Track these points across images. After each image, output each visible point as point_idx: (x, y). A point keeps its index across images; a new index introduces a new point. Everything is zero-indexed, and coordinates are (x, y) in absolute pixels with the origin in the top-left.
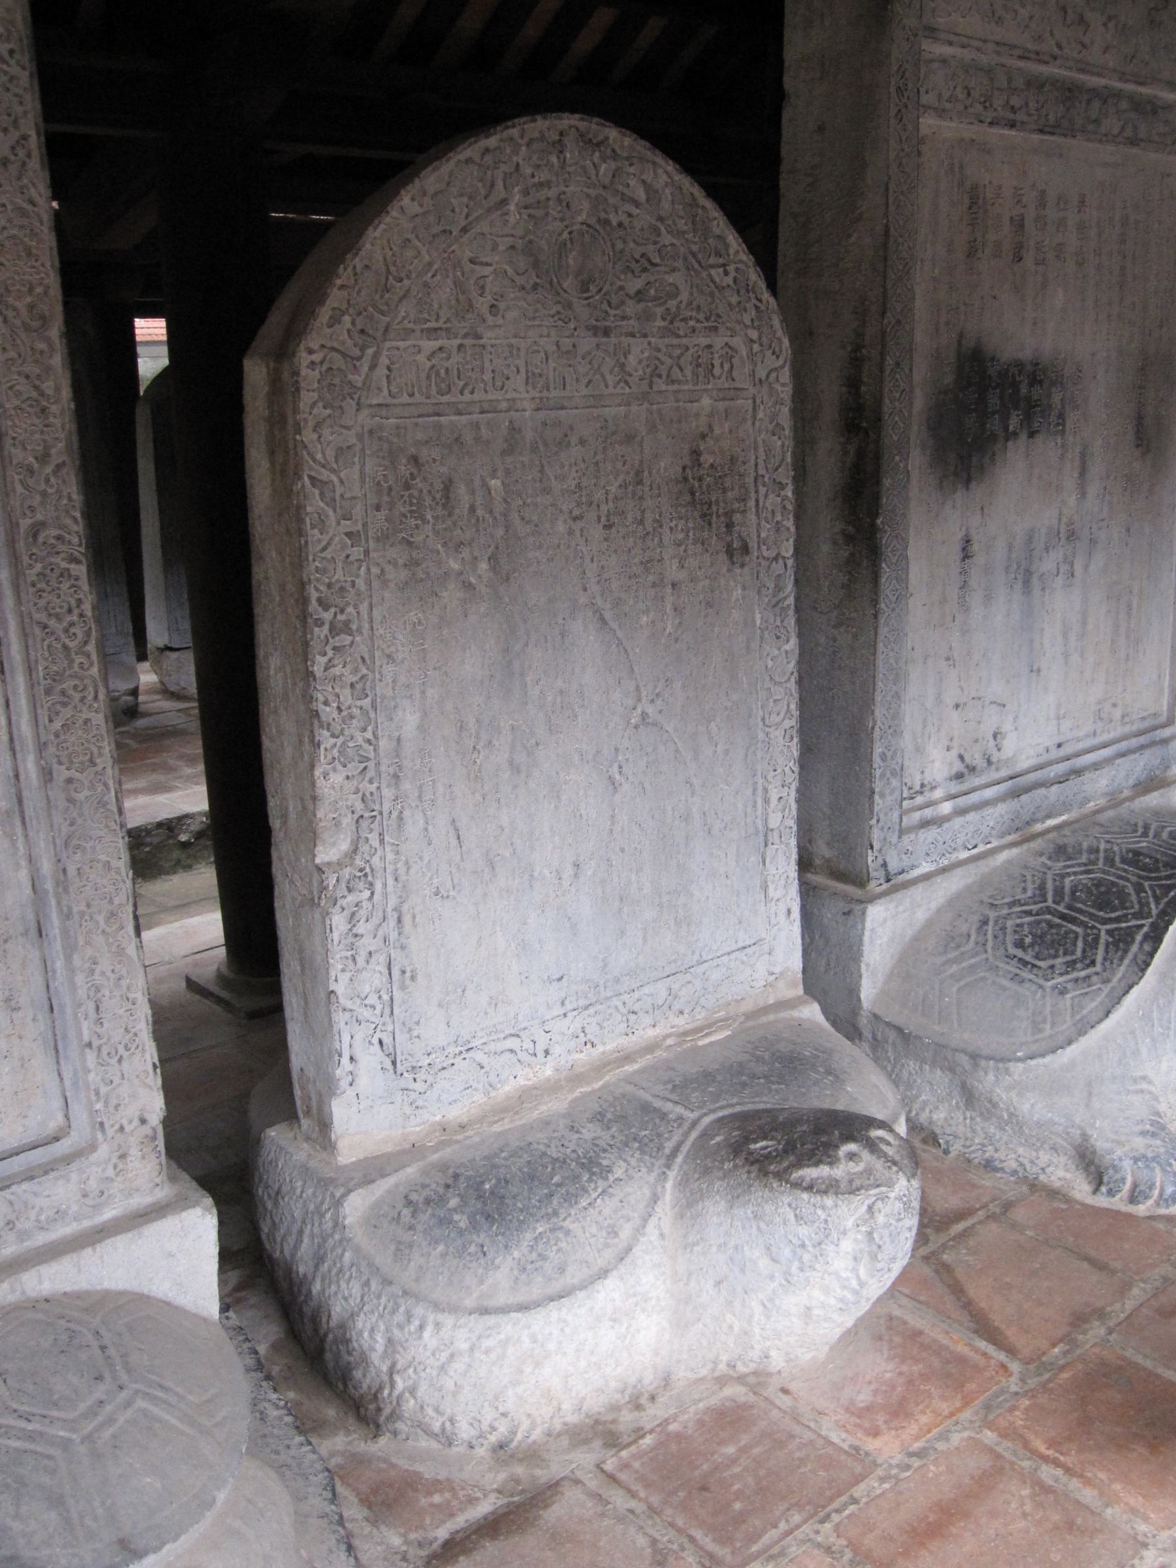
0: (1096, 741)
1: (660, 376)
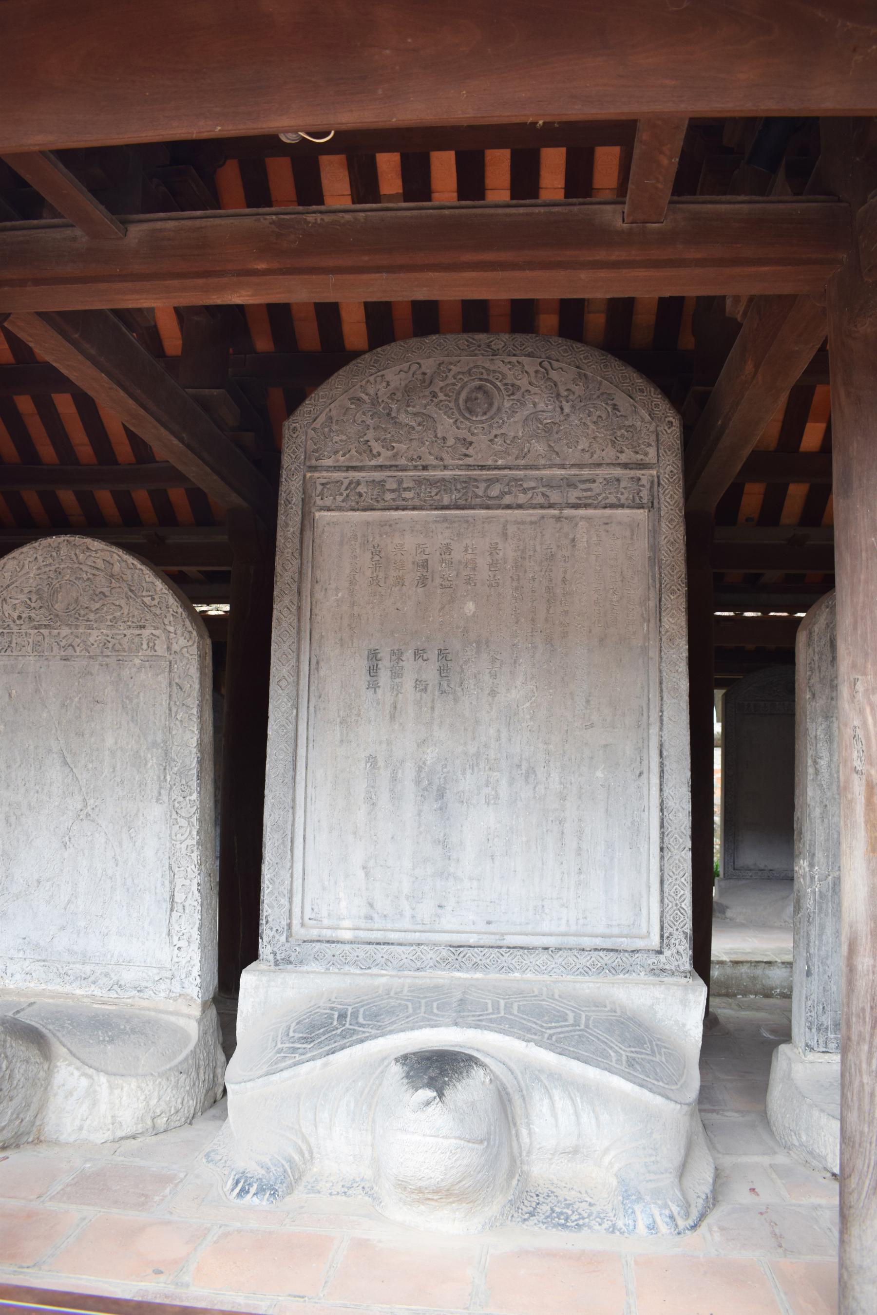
0: (529, 928)
1: (107, 648)
